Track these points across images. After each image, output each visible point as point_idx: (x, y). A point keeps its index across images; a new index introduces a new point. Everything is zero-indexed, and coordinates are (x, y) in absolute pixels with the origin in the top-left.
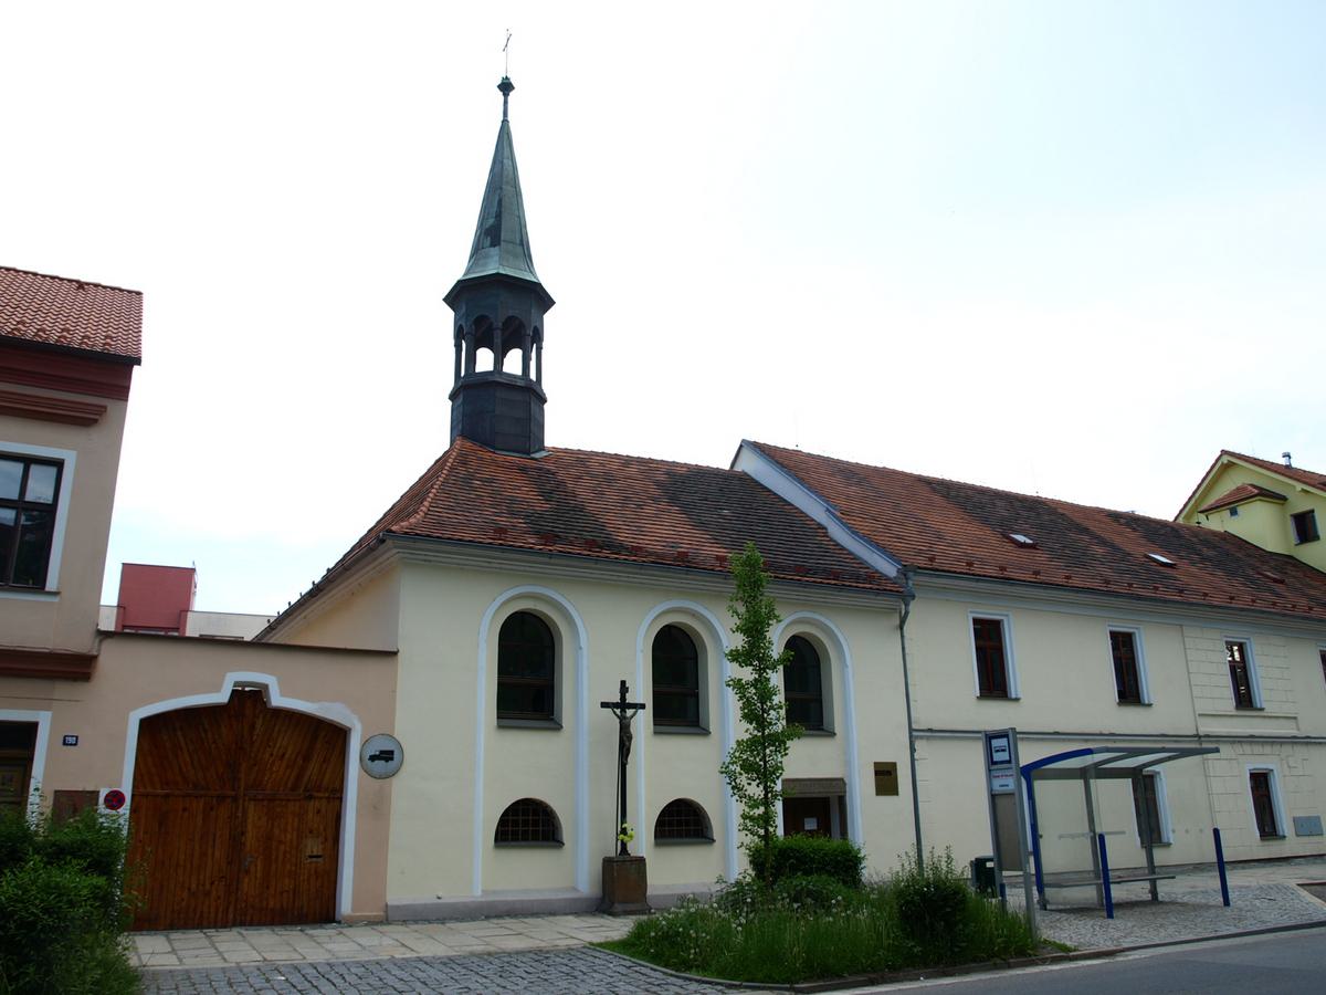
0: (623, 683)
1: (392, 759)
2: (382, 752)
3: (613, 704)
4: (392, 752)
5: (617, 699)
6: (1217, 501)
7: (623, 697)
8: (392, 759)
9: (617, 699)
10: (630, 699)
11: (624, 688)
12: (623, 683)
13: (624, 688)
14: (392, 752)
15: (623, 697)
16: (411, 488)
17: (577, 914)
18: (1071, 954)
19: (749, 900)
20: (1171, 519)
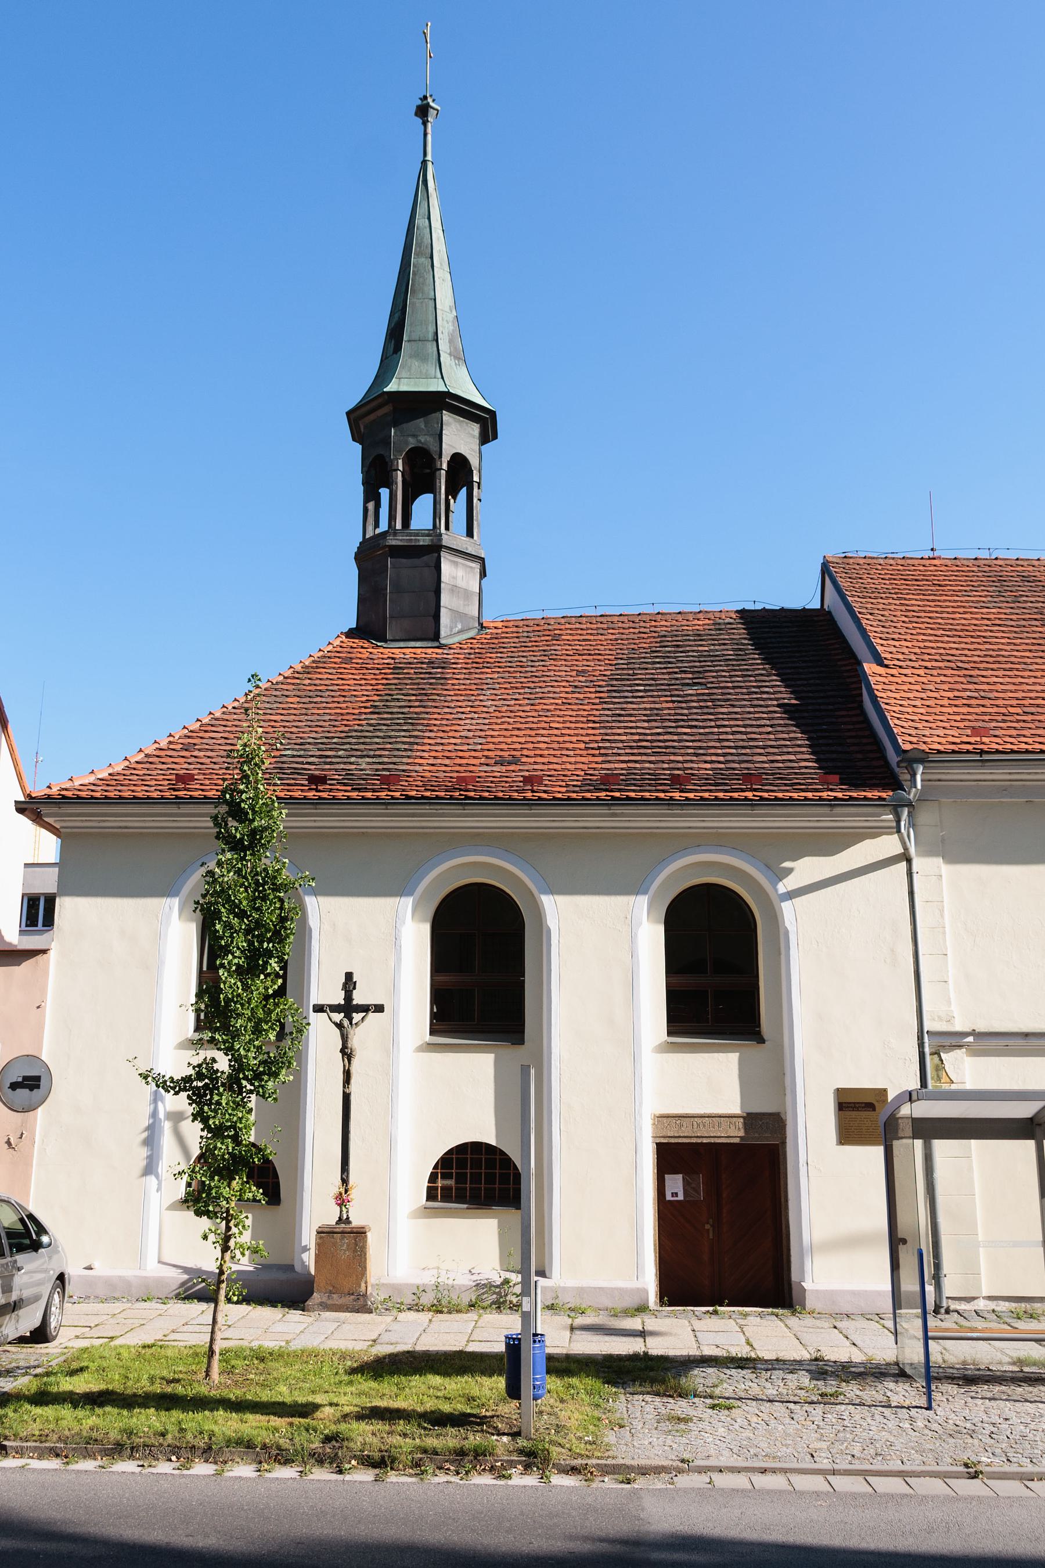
0: (349, 976)
1: (38, 1087)
2: (25, 1078)
3: (330, 1006)
4: (38, 1079)
5: (339, 999)
6: (581, 1291)
7: (348, 997)
8: (38, 1087)
9: (339, 999)
10: (358, 999)
11: (349, 983)
12: (349, 976)
13: (349, 983)
14: (38, 1079)
15: (348, 997)
16: (782, 610)
17: (28, 1299)
18: (854, 692)
19: (204, 1195)
20: (355, 626)
